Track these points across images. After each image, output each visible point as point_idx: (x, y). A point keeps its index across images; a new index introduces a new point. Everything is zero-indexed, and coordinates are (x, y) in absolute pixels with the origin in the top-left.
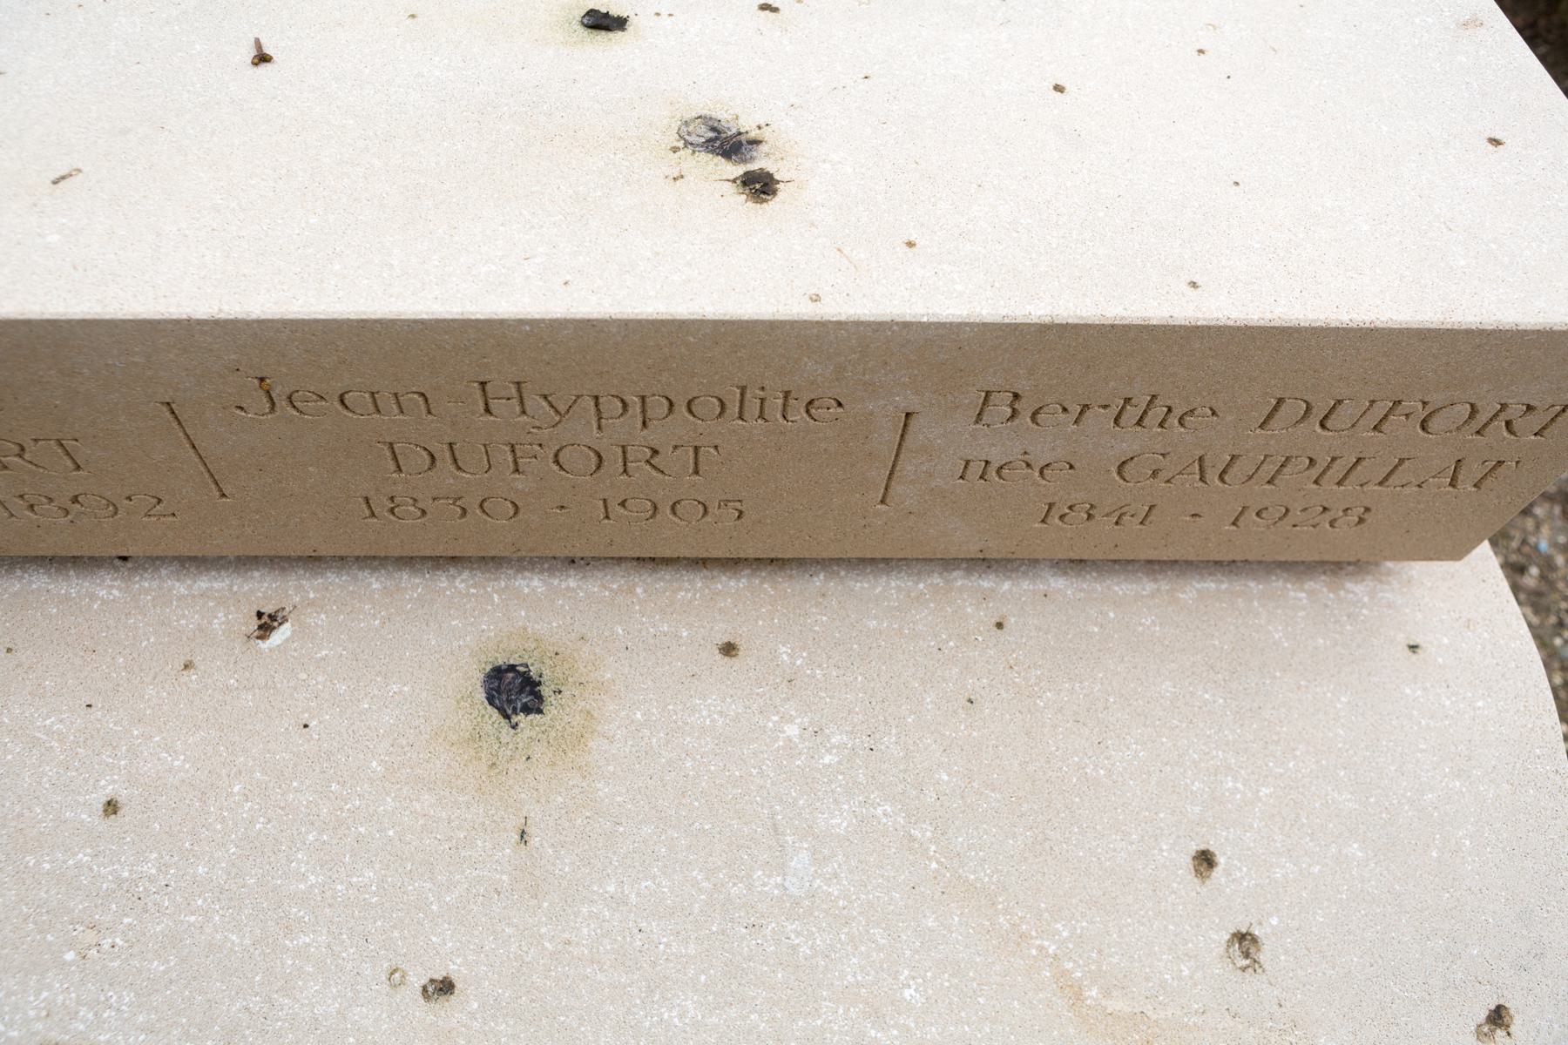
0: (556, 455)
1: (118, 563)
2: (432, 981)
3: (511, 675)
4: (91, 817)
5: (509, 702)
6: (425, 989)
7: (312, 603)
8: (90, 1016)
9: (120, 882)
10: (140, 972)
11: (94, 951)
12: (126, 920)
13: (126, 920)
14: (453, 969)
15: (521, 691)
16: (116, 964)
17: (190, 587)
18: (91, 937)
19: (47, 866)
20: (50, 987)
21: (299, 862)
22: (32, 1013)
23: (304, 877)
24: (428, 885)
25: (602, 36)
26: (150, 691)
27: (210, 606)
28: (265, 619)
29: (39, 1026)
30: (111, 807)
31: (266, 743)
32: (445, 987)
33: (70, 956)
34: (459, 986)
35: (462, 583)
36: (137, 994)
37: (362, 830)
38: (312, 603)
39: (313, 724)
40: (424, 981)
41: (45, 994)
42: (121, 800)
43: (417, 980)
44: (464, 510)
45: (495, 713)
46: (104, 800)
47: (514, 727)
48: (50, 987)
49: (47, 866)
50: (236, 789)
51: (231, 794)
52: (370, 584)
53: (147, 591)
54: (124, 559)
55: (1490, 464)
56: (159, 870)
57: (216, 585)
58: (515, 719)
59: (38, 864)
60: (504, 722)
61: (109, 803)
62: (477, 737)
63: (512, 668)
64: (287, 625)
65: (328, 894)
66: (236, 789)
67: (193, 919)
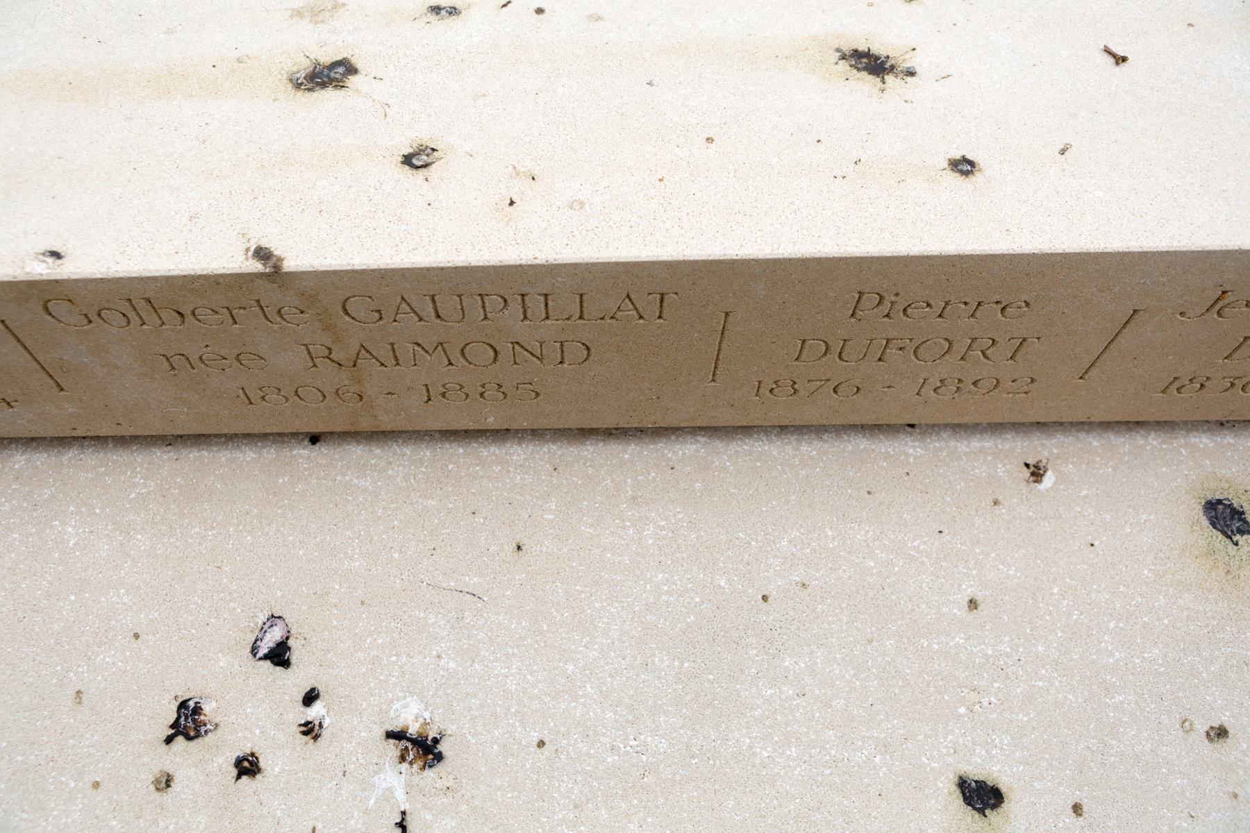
0: (589, 355)
1: (910, 429)
2: (1212, 728)
3: (1221, 507)
4: (961, 611)
5: (1227, 526)
6: (1208, 734)
7: (1058, 457)
8: (983, 752)
9: (987, 657)
10: (1011, 721)
11: (977, 707)
12: (996, 685)
13: (996, 685)
14: (1225, 719)
15: (1232, 518)
16: (994, 716)
17: (968, 446)
18: (974, 696)
19: (936, 646)
20: (953, 733)
21: (1106, 642)
22: (944, 751)
23: (1111, 654)
24: (1197, 659)
25: (878, 49)
26: (978, 521)
27: (991, 460)
28: (1032, 469)
29: (950, 760)
30: (973, 604)
31: (136, 563)
32: (1221, 733)
33: (962, 710)
34: (1231, 731)
35: (1152, 442)
36: (1012, 738)
37: (1146, 619)
38: (1058, 457)
39: (1096, 543)
40: (1206, 728)
41: (950, 737)
42: (979, 598)
43: (1202, 728)
44: (467, 395)
45: (1220, 536)
46: (967, 599)
47: (1236, 544)
48: (953, 733)
49: (936, 646)
50: (1055, 590)
51: (1052, 594)
52: (1090, 443)
53: (941, 449)
54: (912, 426)
55: (1017, 342)
56: (1012, 649)
57: (986, 444)
58: (1235, 538)
59: (930, 645)
60: (1228, 541)
61: (971, 601)
62: (1212, 552)
63: (1219, 502)
64: (1049, 473)
65: (1130, 665)
66: (1055, 590)
67: (1040, 684)
